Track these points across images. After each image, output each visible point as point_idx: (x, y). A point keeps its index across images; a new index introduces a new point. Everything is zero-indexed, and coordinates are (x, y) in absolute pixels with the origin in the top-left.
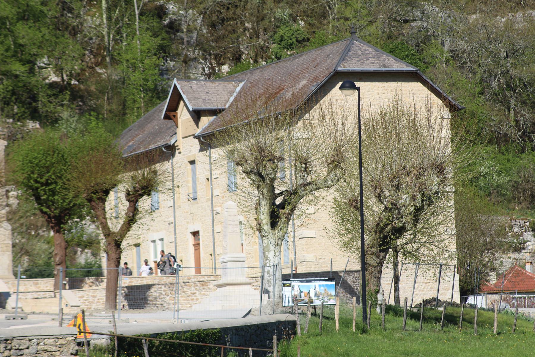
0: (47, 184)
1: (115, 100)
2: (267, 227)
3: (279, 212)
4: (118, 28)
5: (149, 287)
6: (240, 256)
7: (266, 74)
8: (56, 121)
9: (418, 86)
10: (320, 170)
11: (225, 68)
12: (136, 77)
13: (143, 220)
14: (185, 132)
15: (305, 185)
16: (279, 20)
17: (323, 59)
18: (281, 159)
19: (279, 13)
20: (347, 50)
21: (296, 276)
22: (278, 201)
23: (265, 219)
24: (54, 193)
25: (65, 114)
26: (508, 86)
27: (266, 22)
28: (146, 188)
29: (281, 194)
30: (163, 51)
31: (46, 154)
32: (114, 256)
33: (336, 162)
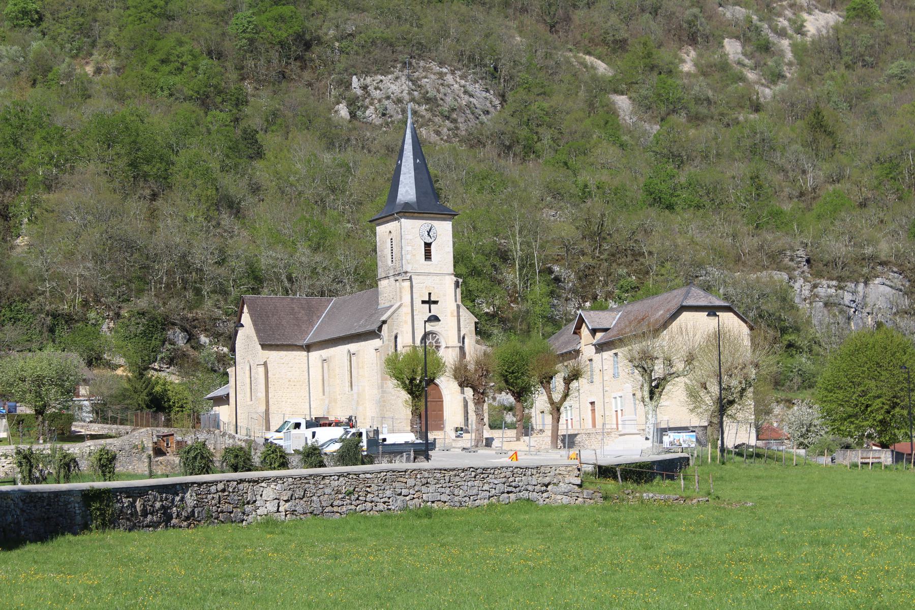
0: (513, 373)
1: (524, 323)
2: (647, 400)
3: (655, 390)
4: (527, 280)
5: (576, 435)
6: (633, 417)
7: (637, 308)
8: (490, 335)
9: (731, 314)
10: (679, 366)
11: (588, 304)
12: (537, 309)
13: (573, 394)
14: (586, 344)
15: (671, 374)
16: (621, 276)
17: (675, 298)
18: (657, 358)
19: (620, 271)
20: (688, 293)
21: (671, 429)
22: (653, 384)
23: (647, 395)
24: (517, 378)
25: (496, 332)
26: (760, 316)
27: (612, 276)
28: (575, 375)
29: (655, 380)
30: (552, 294)
31: (512, 355)
32: (556, 416)
33: (690, 359)
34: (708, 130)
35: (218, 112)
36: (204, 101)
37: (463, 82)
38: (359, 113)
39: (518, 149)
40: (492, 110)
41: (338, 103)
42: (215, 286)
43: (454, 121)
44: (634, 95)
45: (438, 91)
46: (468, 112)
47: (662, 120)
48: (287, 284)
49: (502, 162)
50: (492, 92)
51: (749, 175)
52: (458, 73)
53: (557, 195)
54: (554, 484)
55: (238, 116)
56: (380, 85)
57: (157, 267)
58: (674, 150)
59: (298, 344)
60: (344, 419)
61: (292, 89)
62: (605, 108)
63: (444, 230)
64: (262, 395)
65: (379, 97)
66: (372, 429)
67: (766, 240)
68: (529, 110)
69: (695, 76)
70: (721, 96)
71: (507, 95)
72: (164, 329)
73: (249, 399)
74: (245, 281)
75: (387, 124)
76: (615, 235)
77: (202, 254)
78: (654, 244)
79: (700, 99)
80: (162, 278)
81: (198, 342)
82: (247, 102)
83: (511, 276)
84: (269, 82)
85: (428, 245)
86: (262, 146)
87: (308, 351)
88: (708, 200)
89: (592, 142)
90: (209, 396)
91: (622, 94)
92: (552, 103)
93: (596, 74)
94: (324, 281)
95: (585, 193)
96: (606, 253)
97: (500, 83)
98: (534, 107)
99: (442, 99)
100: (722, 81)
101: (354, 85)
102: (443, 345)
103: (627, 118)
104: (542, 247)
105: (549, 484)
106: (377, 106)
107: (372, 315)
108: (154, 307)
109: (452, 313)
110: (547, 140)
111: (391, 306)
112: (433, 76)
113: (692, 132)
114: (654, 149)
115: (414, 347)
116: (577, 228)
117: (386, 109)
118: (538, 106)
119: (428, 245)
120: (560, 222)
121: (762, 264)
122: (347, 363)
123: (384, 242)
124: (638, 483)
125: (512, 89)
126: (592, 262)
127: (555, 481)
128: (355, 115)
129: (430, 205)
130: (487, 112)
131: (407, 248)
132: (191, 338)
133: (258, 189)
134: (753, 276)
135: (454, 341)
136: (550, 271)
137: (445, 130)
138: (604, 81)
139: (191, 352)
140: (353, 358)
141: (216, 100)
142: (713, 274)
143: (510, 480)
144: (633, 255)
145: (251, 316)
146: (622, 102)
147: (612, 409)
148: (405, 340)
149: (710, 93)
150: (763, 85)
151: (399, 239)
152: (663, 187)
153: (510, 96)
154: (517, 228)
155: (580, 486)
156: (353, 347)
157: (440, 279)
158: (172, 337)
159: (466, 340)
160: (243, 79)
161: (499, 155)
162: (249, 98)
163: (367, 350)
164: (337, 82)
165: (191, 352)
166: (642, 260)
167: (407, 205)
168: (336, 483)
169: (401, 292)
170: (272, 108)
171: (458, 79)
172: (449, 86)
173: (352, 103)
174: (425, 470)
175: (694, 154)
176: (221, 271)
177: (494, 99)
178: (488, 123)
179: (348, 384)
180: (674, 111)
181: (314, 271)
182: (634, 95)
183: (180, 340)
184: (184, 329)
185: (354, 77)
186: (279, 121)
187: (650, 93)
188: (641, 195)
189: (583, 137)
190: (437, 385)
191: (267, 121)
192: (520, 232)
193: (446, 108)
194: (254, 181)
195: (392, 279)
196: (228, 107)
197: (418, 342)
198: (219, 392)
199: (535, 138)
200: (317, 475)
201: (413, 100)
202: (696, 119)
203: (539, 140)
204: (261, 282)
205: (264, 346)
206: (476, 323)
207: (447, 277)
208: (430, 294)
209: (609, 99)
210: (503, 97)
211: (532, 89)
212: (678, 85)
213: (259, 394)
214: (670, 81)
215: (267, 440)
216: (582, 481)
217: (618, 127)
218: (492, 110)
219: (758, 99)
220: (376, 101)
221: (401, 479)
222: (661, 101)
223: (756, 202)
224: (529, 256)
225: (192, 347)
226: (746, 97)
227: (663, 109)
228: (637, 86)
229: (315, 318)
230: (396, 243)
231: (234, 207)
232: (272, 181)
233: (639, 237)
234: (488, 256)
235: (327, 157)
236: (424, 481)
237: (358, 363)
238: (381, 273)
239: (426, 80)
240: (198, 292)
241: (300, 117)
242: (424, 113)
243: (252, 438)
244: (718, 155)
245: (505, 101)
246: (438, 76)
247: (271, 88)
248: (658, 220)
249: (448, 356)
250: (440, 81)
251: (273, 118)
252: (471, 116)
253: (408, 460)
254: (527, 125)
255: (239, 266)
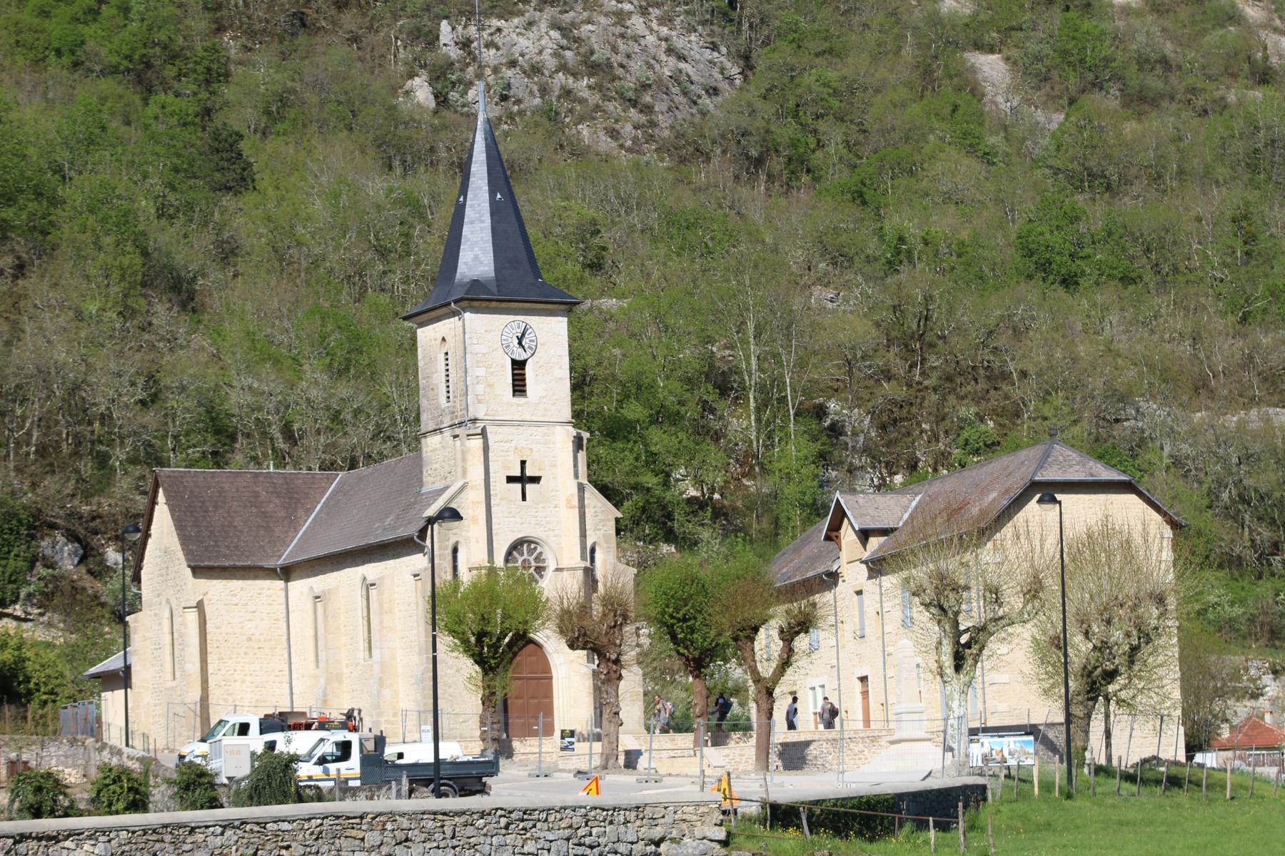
0: (684, 620)
2: (950, 671)
3: (964, 653)
8: (696, 544)
9: (1132, 498)
10: (1014, 601)
11: (898, 479)
12: (790, 490)
13: (800, 662)
18: (967, 588)
19: (963, 412)
20: (1047, 455)
21: (986, 730)
23: (948, 661)
25: (706, 534)
27: (947, 422)
28: (803, 624)
31: (683, 584)
32: (765, 706)
33: (1034, 591)
34: (1161, 124)
35: (170, 98)
36: (142, 74)
37: (664, 31)
38: (453, 95)
39: (776, 164)
40: (724, 86)
41: (411, 76)
42: (135, 449)
43: (647, 109)
44: (1015, 53)
45: (615, 49)
46: (676, 90)
47: (1072, 102)
48: (281, 445)
49: (744, 191)
50: (724, 50)
51: (1229, 214)
52: (655, 12)
53: (841, 258)
54: (673, 840)
55: (209, 104)
56: (497, 39)
57: (19, 412)
58: (1092, 163)
59: (266, 564)
60: (336, 715)
61: (320, 49)
62: (956, 80)
63: (551, 333)
64: (194, 667)
65: (493, 62)
66: (371, 735)
67: (1256, 346)
68: (798, 85)
69: (1139, 13)
70: (1191, 55)
71: (754, 55)
72: (33, 537)
73: (169, 677)
74: (196, 438)
75: (511, 117)
76: (954, 340)
77: (112, 388)
78: (1032, 355)
79: (1147, 61)
80: (29, 434)
81: (102, 562)
82: (227, 75)
83: (741, 423)
84: (272, 35)
85: (518, 366)
86: (250, 165)
87: (287, 580)
88: (1143, 266)
89: (927, 149)
90: (93, 670)
91: (991, 50)
92: (845, 72)
93: (937, 13)
94: (357, 436)
95: (900, 254)
96: (935, 375)
97: (739, 31)
98: (808, 79)
99: (622, 66)
100: (1193, 23)
101: (443, 40)
102: (551, 564)
103: (1000, 99)
104: (801, 365)
105: (662, 840)
106: (491, 79)
107: (410, 506)
108: (13, 493)
109: (568, 501)
110: (834, 148)
111: (446, 488)
112: (603, 20)
113: (1130, 128)
114: (1050, 162)
115: (492, 571)
116: (878, 325)
117: (509, 86)
118: (819, 76)
119: (518, 366)
120: (842, 312)
121: (1250, 393)
122: (360, 602)
123: (432, 360)
124: (871, 840)
125: (766, 43)
126: (902, 393)
127: (675, 834)
128: (446, 100)
129: (520, 285)
130: (713, 91)
131: (476, 372)
132: (88, 554)
133: (233, 252)
134: (1232, 420)
135: (572, 556)
136: (821, 412)
137: (628, 128)
138: (953, 27)
139: (89, 584)
140: (373, 592)
141: (166, 73)
142: (1152, 416)
143: (581, 832)
144: (989, 378)
145: (172, 511)
146: (991, 68)
147: (877, 690)
148: (473, 556)
149: (1168, 48)
150: (1276, 30)
151: (460, 353)
152: (1056, 239)
153: (761, 59)
154: (751, 326)
155: (725, 843)
156: (371, 570)
157: (543, 427)
158: (48, 552)
159: (598, 555)
160: (220, 29)
161: (737, 177)
162: (232, 68)
163: (402, 579)
164: (410, 33)
165: (89, 584)
166: (1006, 388)
167: (476, 284)
168: (219, 841)
169: (464, 460)
170: (279, 88)
171: (654, 25)
172: (636, 39)
173: (441, 76)
174: (403, 815)
175: (1134, 171)
176: (150, 418)
177: (728, 65)
178: (718, 113)
179: (362, 645)
180: (1097, 85)
181: (336, 417)
182: (1015, 53)
183: (66, 557)
184: (72, 537)
185: (444, 23)
186: (291, 114)
187: (1047, 50)
188: (1013, 256)
189: (907, 139)
190: (539, 646)
191: (268, 113)
192: (757, 336)
193: (629, 84)
194: (226, 235)
195: (448, 433)
196: (188, 86)
197: (499, 561)
198: (113, 663)
199: (812, 141)
200: (180, 826)
201: (563, 67)
202: (1140, 101)
203: (820, 145)
204: (233, 438)
205: (198, 571)
206: (617, 520)
207: (559, 428)
208: (523, 463)
209: (963, 61)
210: (746, 60)
211: (806, 44)
212: (1103, 33)
213: (189, 667)
214: (1086, 25)
215: (182, 757)
216: (729, 834)
217: (979, 118)
218: (724, 86)
219: (1266, 58)
220: (488, 71)
221: (354, 833)
222: (1069, 64)
223: (1243, 269)
224: (778, 382)
225: (90, 572)
226: (1242, 55)
227: (1073, 81)
228: (1020, 34)
229: (300, 512)
230: (458, 361)
231: (184, 293)
232: (261, 236)
233: (1002, 341)
234: (690, 382)
235: (377, 186)
236: (400, 835)
237: (381, 605)
238: (427, 422)
239: (590, 27)
240: (102, 461)
241: (332, 106)
242: (585, 94)
243: (152, 754)
244: (1181, 172)
245: (751, 68)
246: (614, 19)
247: (275, 45)
248: (1040, 306)
249: (559, 585)
250: (619, 30)
251: (278, 111)
252: (680, 99)
253: (399, 795)
254: (796, 116)
255: (182, 406)
